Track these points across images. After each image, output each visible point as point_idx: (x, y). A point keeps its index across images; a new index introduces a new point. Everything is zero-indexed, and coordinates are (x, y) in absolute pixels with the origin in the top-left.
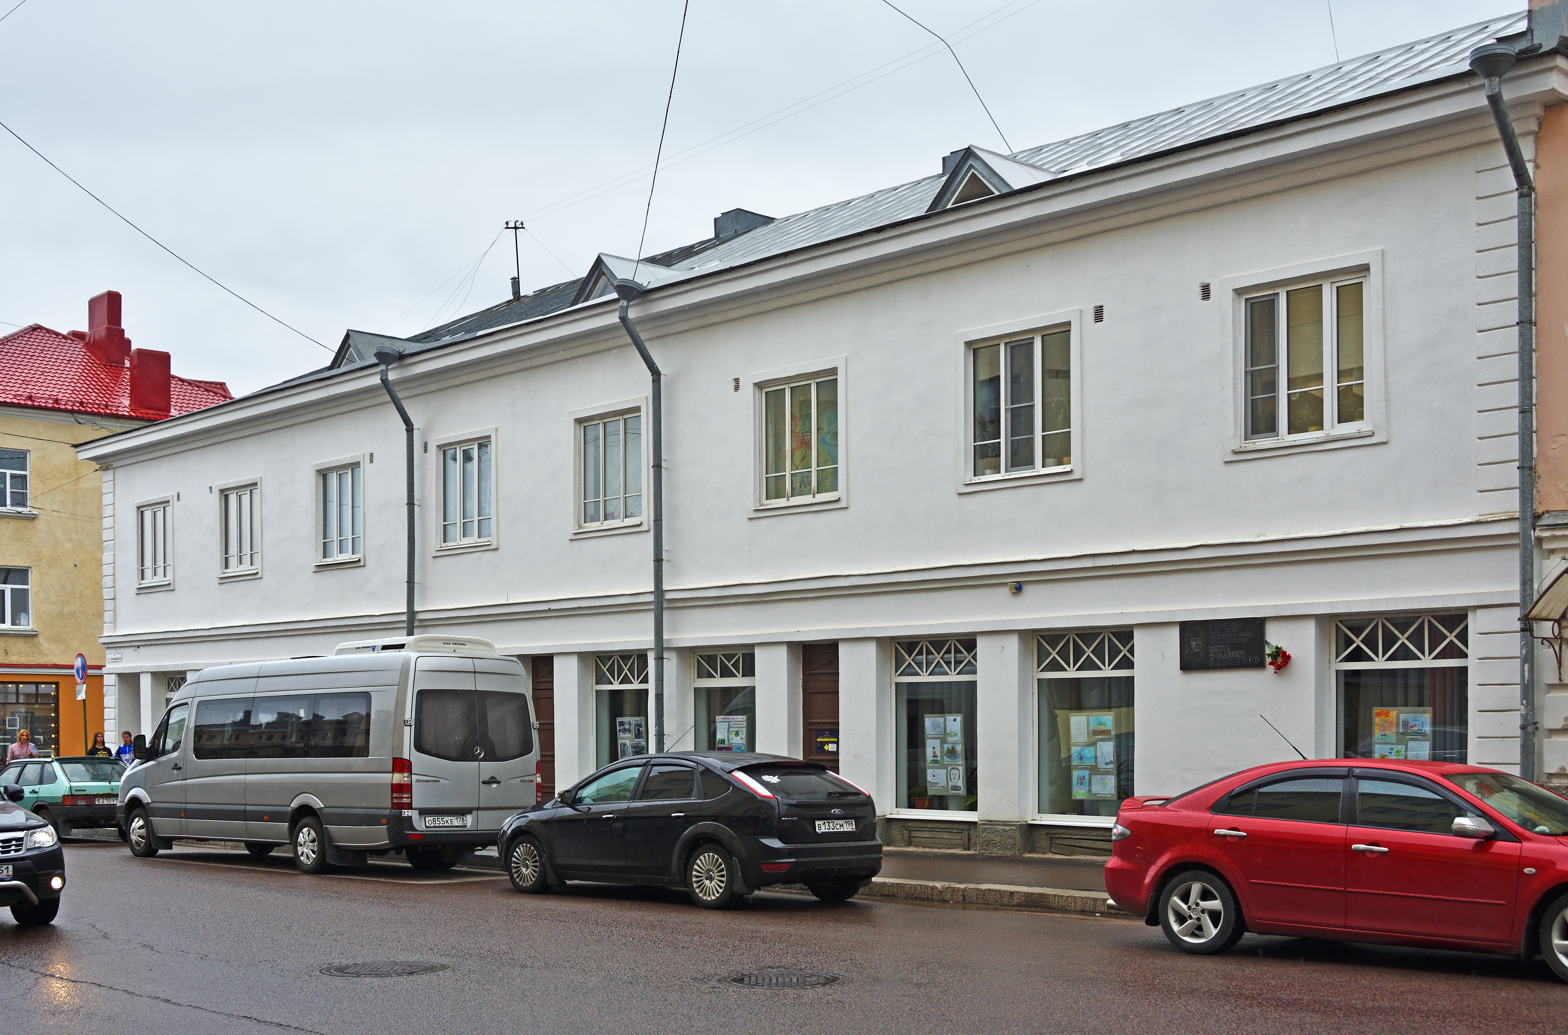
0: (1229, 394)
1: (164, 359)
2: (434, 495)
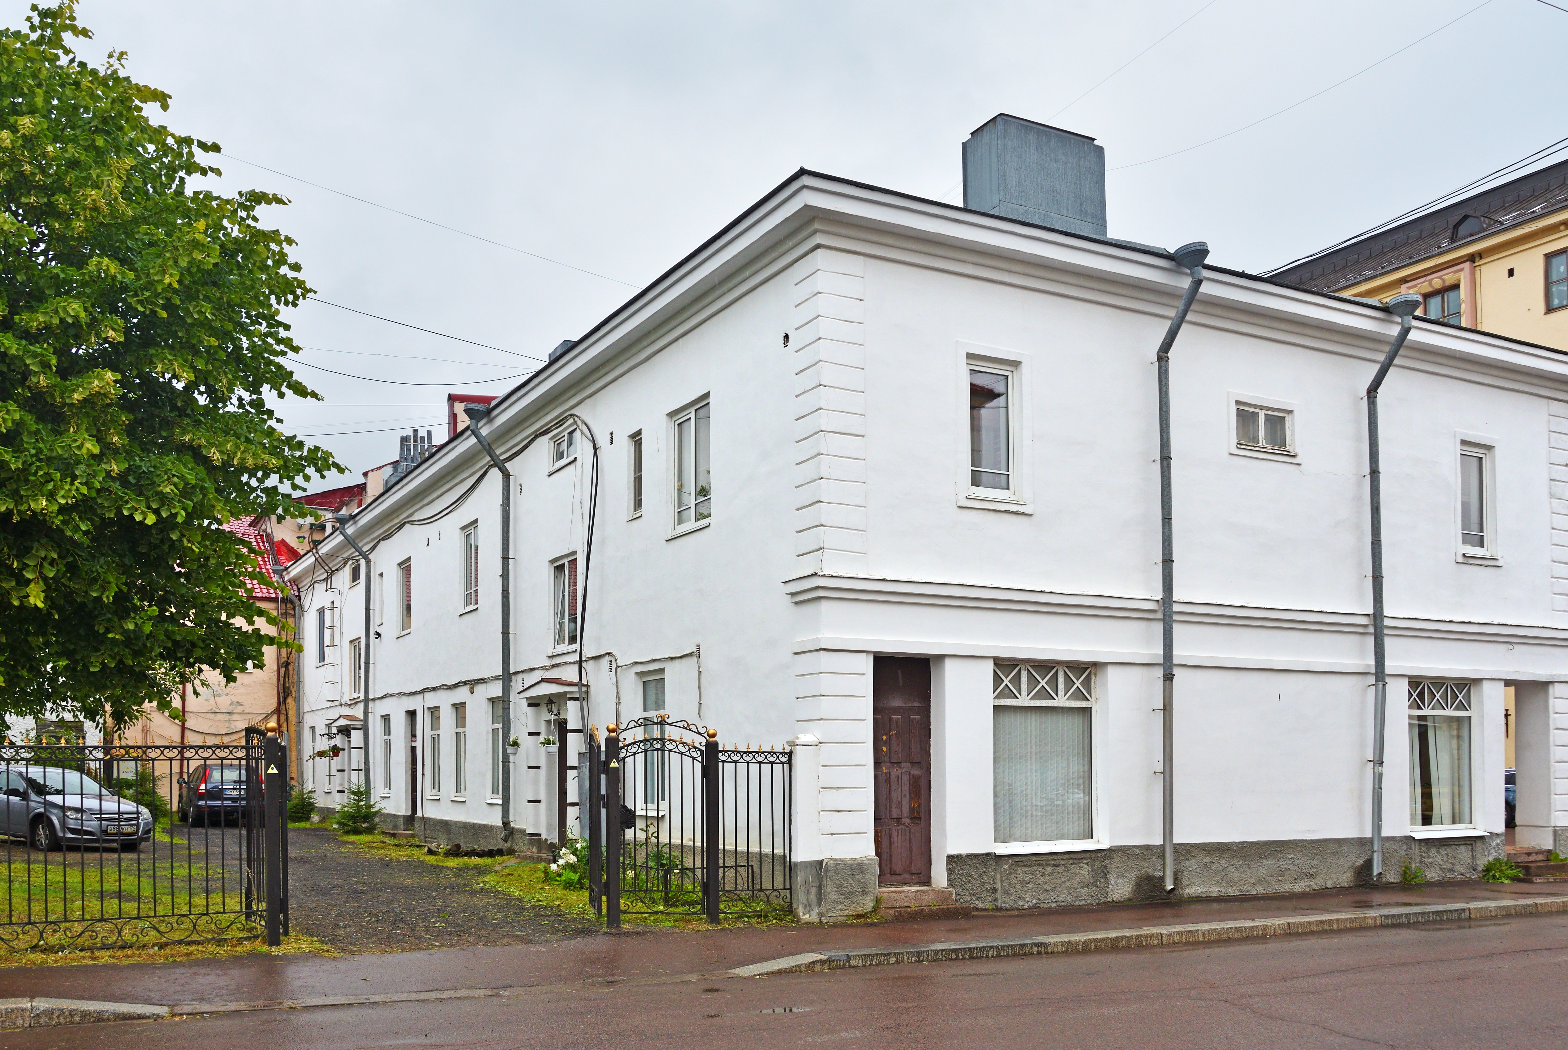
0: (403, 755)
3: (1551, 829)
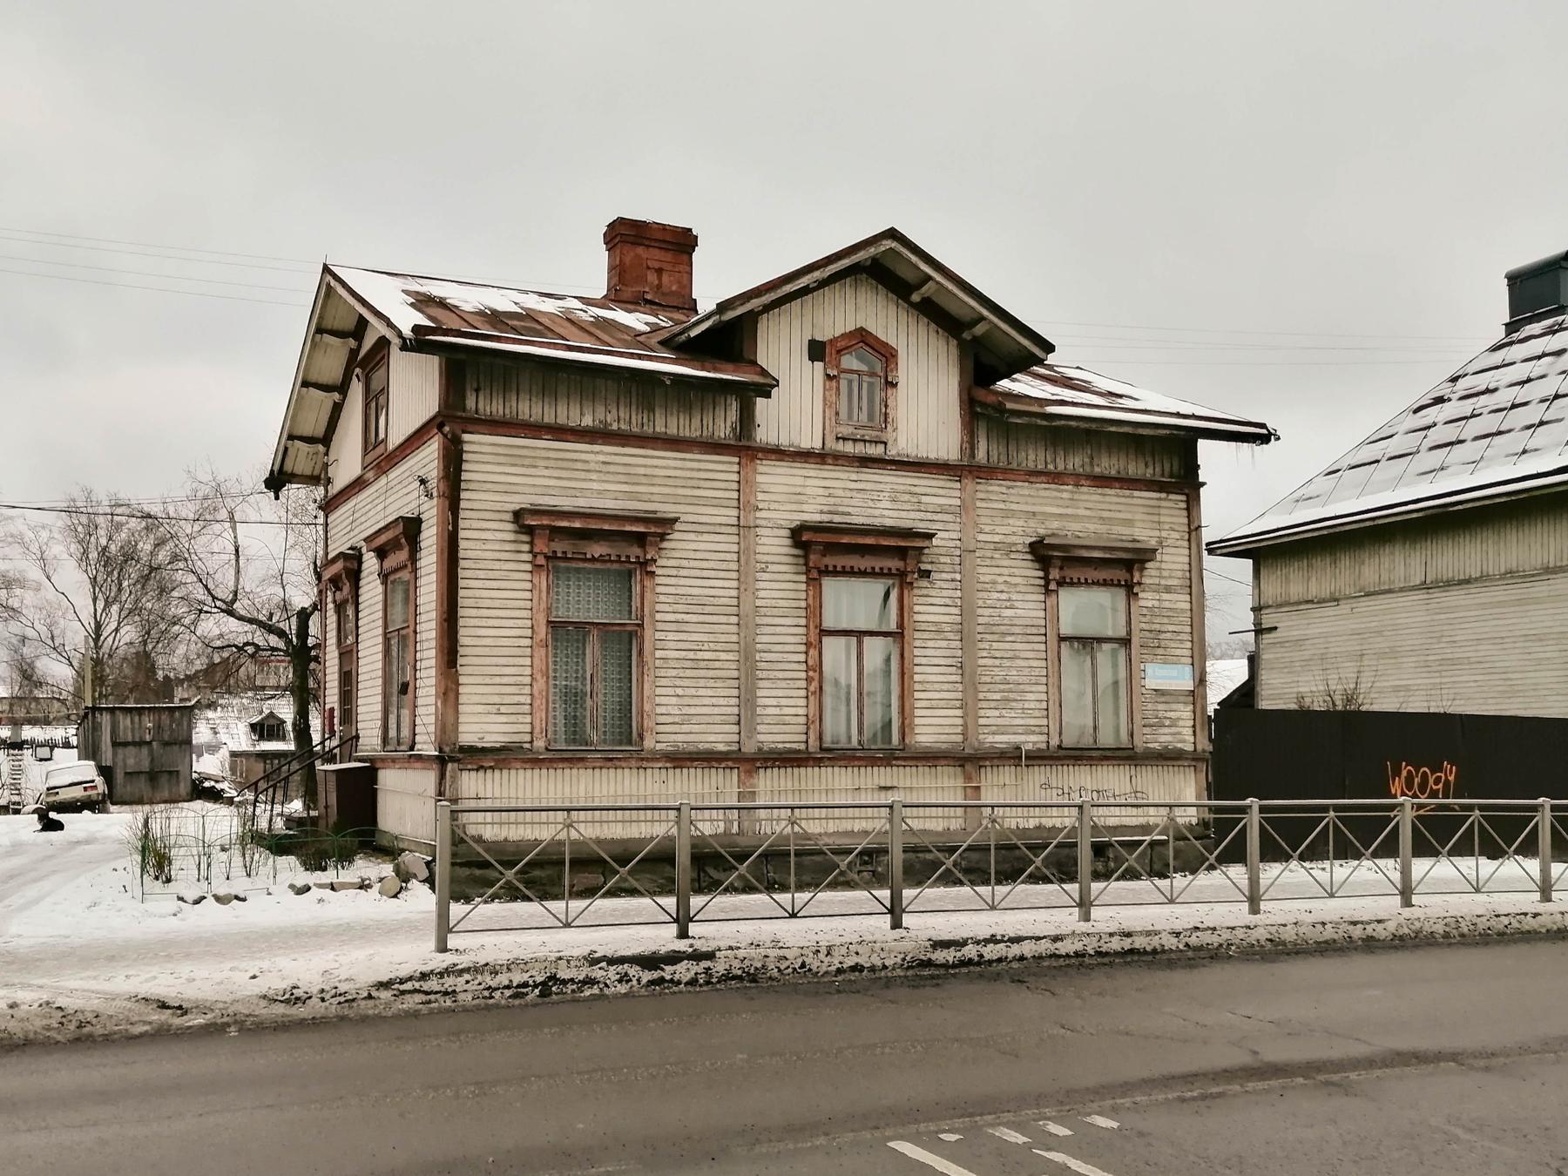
1: (768, 396)
2: (1008, 923)
3: (16, 798)
